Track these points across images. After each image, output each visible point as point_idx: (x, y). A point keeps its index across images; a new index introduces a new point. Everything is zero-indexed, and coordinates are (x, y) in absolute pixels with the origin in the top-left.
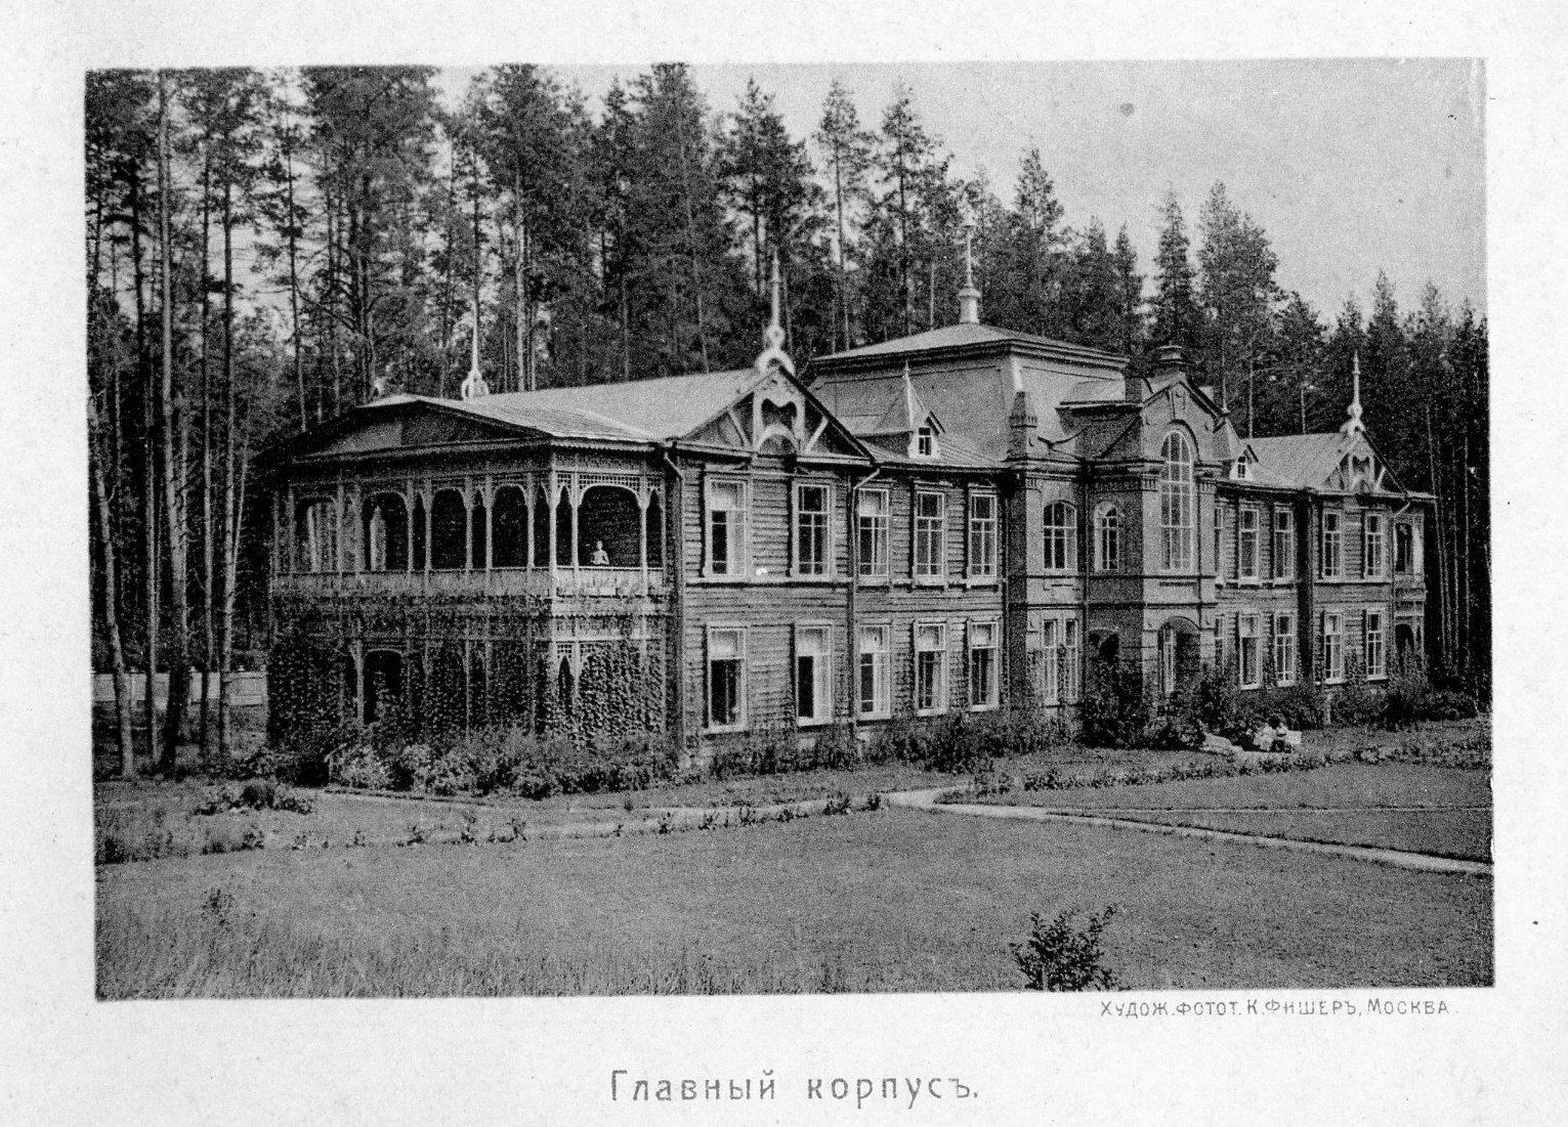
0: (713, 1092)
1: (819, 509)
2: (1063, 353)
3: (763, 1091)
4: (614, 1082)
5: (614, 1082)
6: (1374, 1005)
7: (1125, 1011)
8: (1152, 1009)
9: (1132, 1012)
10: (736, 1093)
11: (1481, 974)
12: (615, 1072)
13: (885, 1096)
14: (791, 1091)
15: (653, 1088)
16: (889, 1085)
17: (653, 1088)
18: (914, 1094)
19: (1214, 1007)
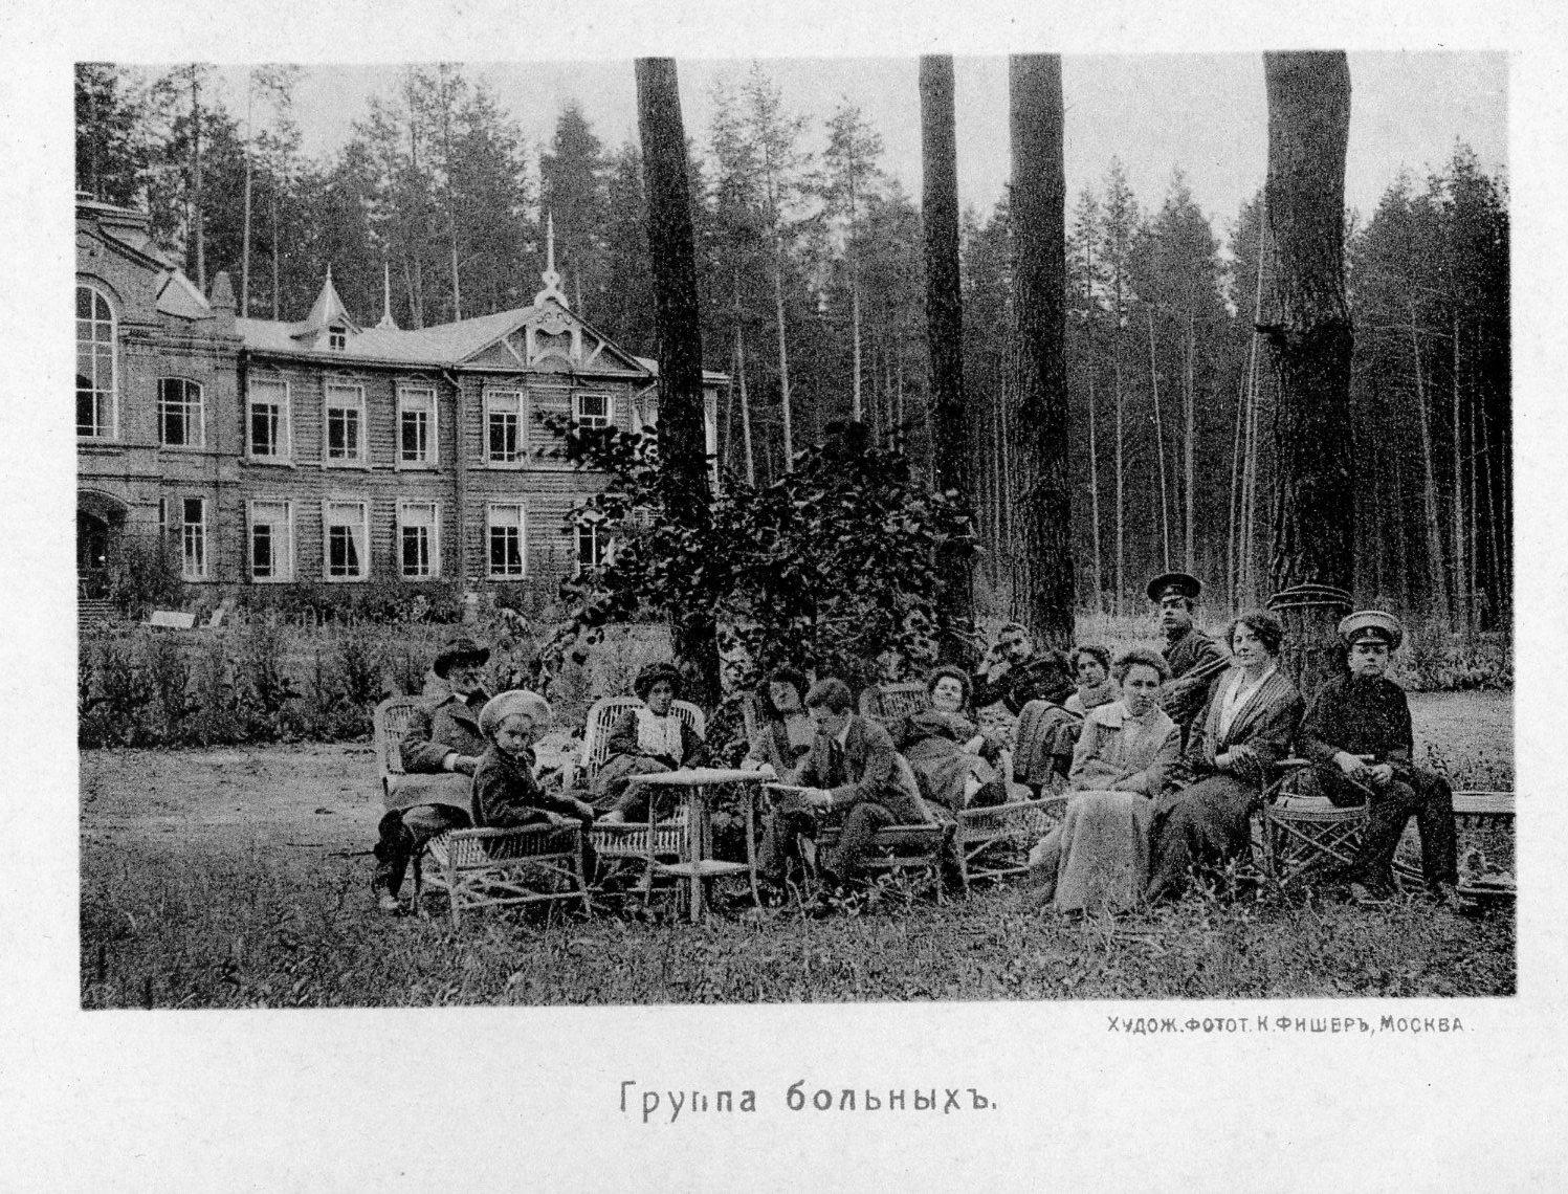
0: (897, 1103)
1: (599, 413)
2: (1236, 553)
3: (901, 1097)
4: (623, 1092)
5: (623, 1092)
6: (252, 769)
7: (1134, 1026)
8: (1160, 1025)
9: (1138, 1027)
10: (922, 1104)
11: (1506, 986)
12: (624, 1084)
13: (695, 1109)
14: (771, 1100)
15: (737, 1099)
16: (725, 1098)
17: (737, 1099)
18: (677, 1108)
19: (1224, 1024)
